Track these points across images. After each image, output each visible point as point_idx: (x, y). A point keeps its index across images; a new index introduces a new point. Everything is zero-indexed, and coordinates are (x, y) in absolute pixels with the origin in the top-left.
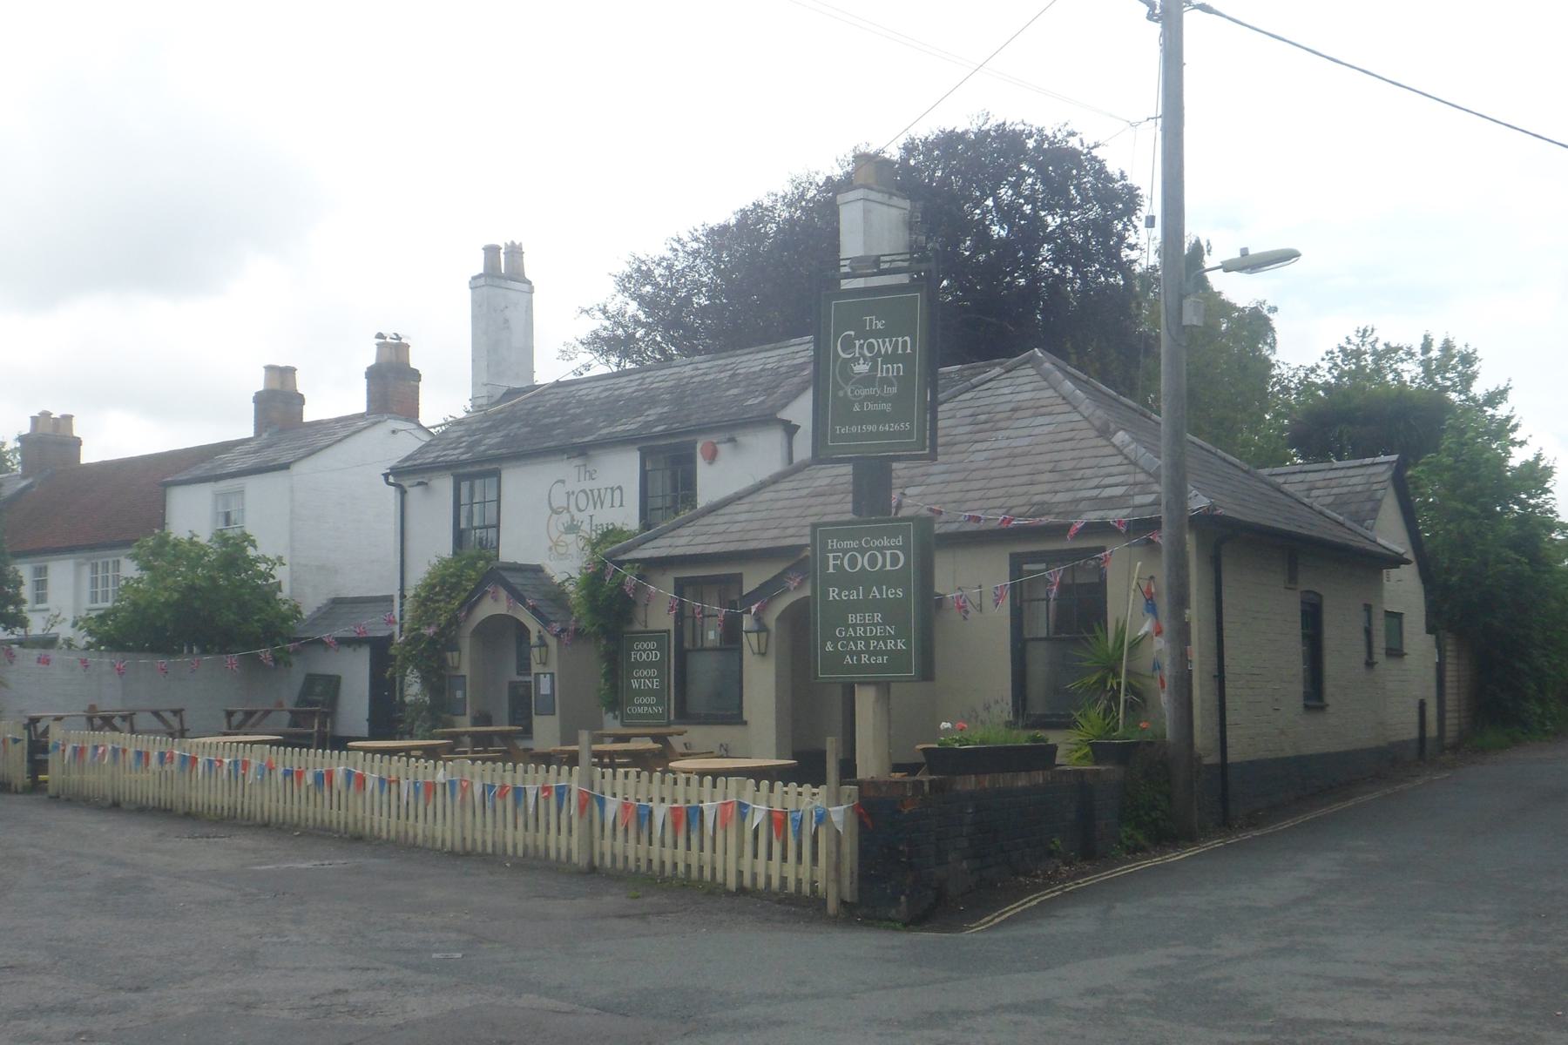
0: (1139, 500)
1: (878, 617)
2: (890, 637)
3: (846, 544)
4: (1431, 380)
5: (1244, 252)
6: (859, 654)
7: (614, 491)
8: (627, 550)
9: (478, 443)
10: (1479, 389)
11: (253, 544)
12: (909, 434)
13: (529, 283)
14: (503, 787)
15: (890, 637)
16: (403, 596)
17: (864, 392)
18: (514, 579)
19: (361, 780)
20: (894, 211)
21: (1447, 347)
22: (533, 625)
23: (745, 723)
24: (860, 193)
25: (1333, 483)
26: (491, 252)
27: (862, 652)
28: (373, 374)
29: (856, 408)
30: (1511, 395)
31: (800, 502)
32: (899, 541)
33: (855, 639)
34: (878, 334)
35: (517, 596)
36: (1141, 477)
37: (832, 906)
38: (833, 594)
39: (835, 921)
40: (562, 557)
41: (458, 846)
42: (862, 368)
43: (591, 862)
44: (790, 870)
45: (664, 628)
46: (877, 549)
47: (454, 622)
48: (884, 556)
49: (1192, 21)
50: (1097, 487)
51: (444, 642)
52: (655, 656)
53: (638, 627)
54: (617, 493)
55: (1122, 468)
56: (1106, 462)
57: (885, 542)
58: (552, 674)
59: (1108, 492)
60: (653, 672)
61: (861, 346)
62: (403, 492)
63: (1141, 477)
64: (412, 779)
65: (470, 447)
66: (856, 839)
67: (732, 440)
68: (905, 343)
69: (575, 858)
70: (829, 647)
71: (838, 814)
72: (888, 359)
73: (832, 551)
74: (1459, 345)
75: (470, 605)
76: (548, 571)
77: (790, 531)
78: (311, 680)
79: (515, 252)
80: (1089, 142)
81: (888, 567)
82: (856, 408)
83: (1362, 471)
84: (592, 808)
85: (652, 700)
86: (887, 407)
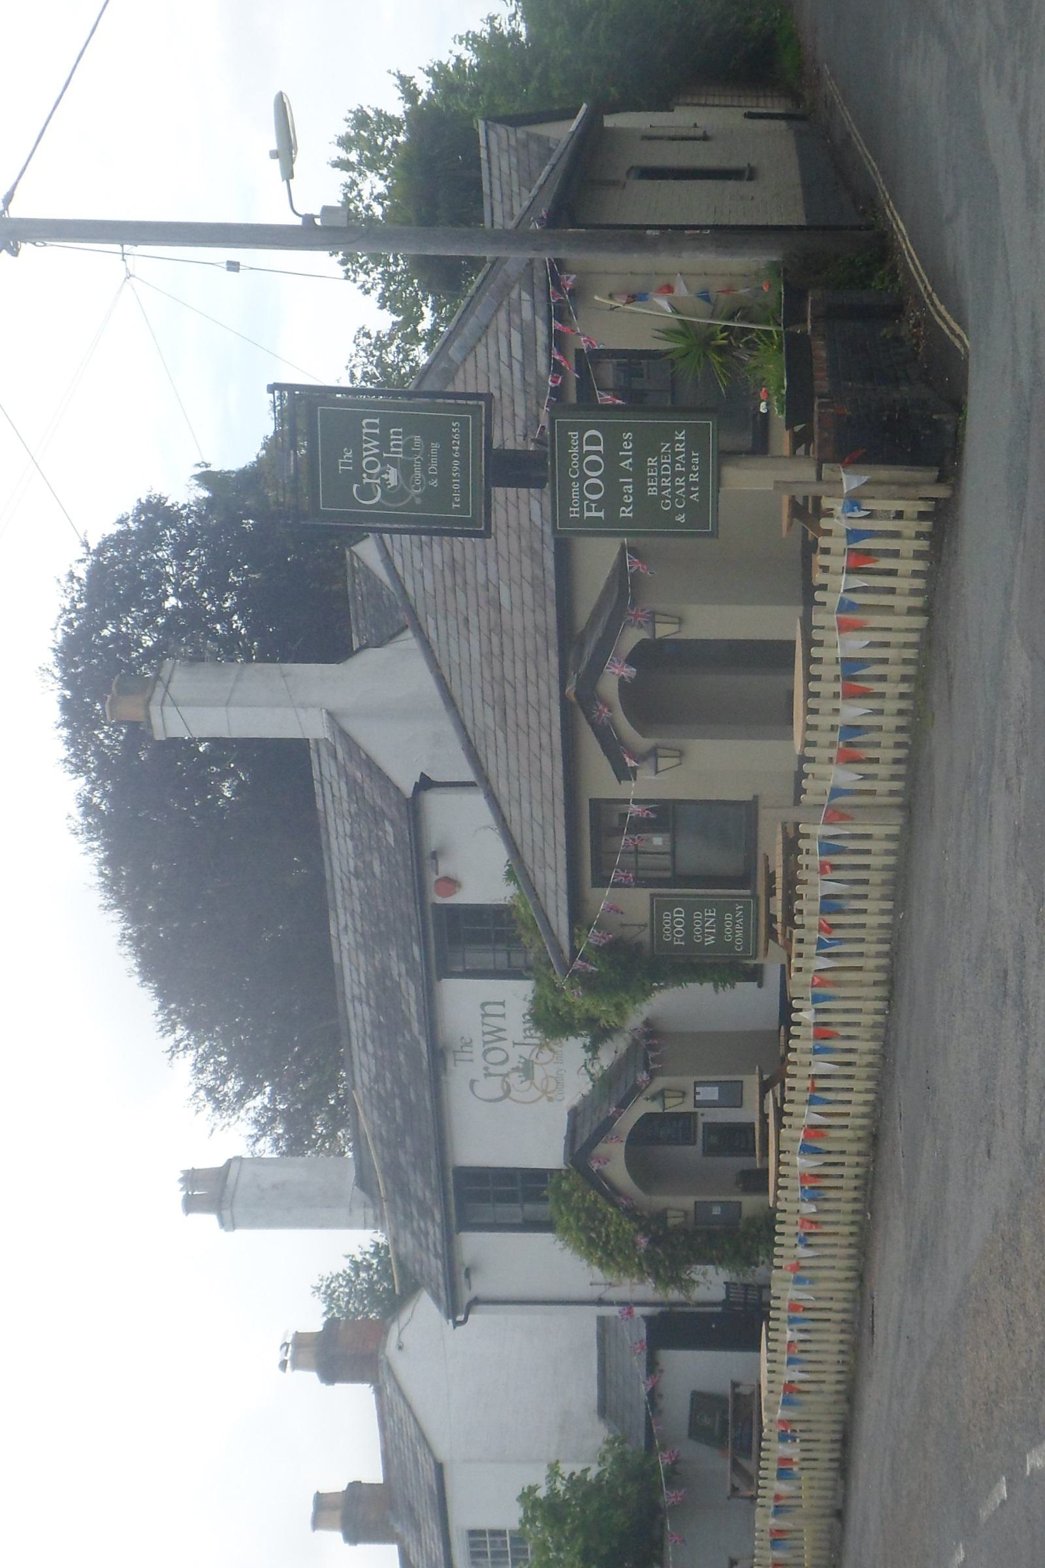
0: (527, 313)
1: (651, 461)
2: (672, 447)
3: (575, 496)
4: (386, 160)
5: (275, 155)
6: (689, 485)
7: (486, 1008)
8: (559, 951)
9: (421, 1204)
10: (397, 108)
11: (533, 1489)
12: (464, 423)
13: (230, 1161)
14: (821, 929)
15: (672, 447)
16: (600, 1302)
17: (418, 473)
18: (585, 1134)
19: (814, 1130)
20: (177, 676)
21: (346, 143)
22: (642, 1107)
23: (756, 797)
24: (154, 710)
25: (507, 191)
26: (191, 1205)
27: (686, 480)
28: (330, 1374)
29: (434, 483)
30: (406, 72)
31: (512, 739)
32: (574, 435)
33: (675, 488)
34: (358, 458)
35: (604, 1130)
36: (502, 315)
37: (942, 492)
38: (626, 513)
39: (956, 487)
40: (559, 1082)
41: (880, 991)
42: (392, 476)
43: (900, 807)
44: (908, 546)
45: (647, 901)
46: (581, 461)
47: (631, 1213)
48: (589, 453)
49: (16, 211)
50: (510, 366)
51: (654, 1225)
52: (679, 914)
53: (645, 936)
54: (489, 1009)
55: (491, 342)
56: (482, 364)
57: (576, 450)
58: (696, 1084)
59: (517, 353)
60: (697, 916)
61: (370, 476)
62: (476, 1301)
63: (502, 315)
64: (810, 1057)
65: (425, 1212)
66: (877, 466)
67: (434, 855)
68: (370, 426)
69: (894, 830)
70: (681, 518)
71: (850, 481)
72: (384, 446)
73: (582, 512)
74: (345, 129)
75: (611, 1193)
76: (575, 1102)
77: (545, 739)
78: (696, 1431)
79: (192, 1178)
80: (81, 552)
81: (601, 448)
82: (434, 483)
83: (494, 161)
84: (843, 806)
85: (728, 917)
86: (435, 446)
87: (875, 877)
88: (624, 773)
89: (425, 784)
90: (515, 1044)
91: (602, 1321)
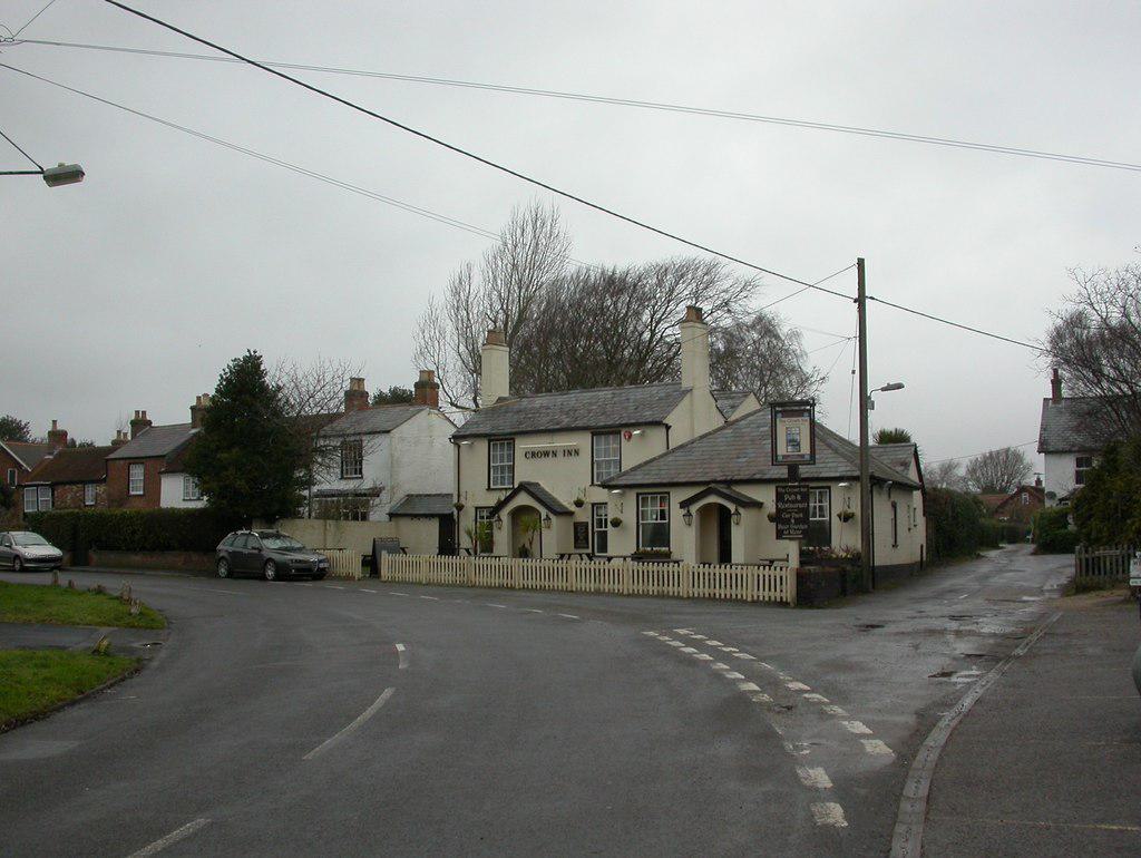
37: (792, 604)
44: (772, 593)
87: (772, 593)
88: (685, 504)
89: (668, 428)
90: (895, 545)
91: (452, 495)
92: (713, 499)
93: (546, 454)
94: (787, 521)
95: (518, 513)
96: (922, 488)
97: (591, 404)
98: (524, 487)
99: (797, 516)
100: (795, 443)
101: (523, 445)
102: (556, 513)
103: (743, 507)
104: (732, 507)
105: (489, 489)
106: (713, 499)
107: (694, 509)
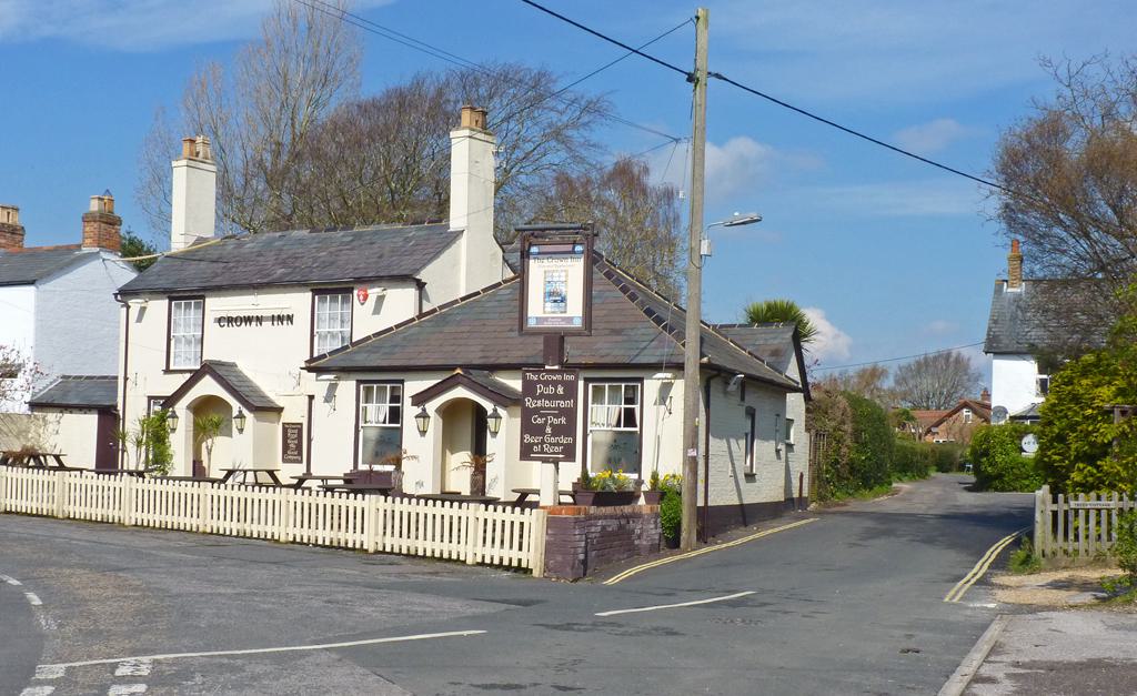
87: (364, 537)
92: (460, 392)
93: (248, 320)
94: (539, 431)
95: (204, 406)
96: (805, 389)
97: (319, 250)
98: (208, 369)
99: (556, 421)
100: (558, 298)
101: (216, 305)
102: (255, 409)
103: (505, 406)
104: (488, 406)
105: (168, 371)
106: (460, 392)
107: (432, 407)
